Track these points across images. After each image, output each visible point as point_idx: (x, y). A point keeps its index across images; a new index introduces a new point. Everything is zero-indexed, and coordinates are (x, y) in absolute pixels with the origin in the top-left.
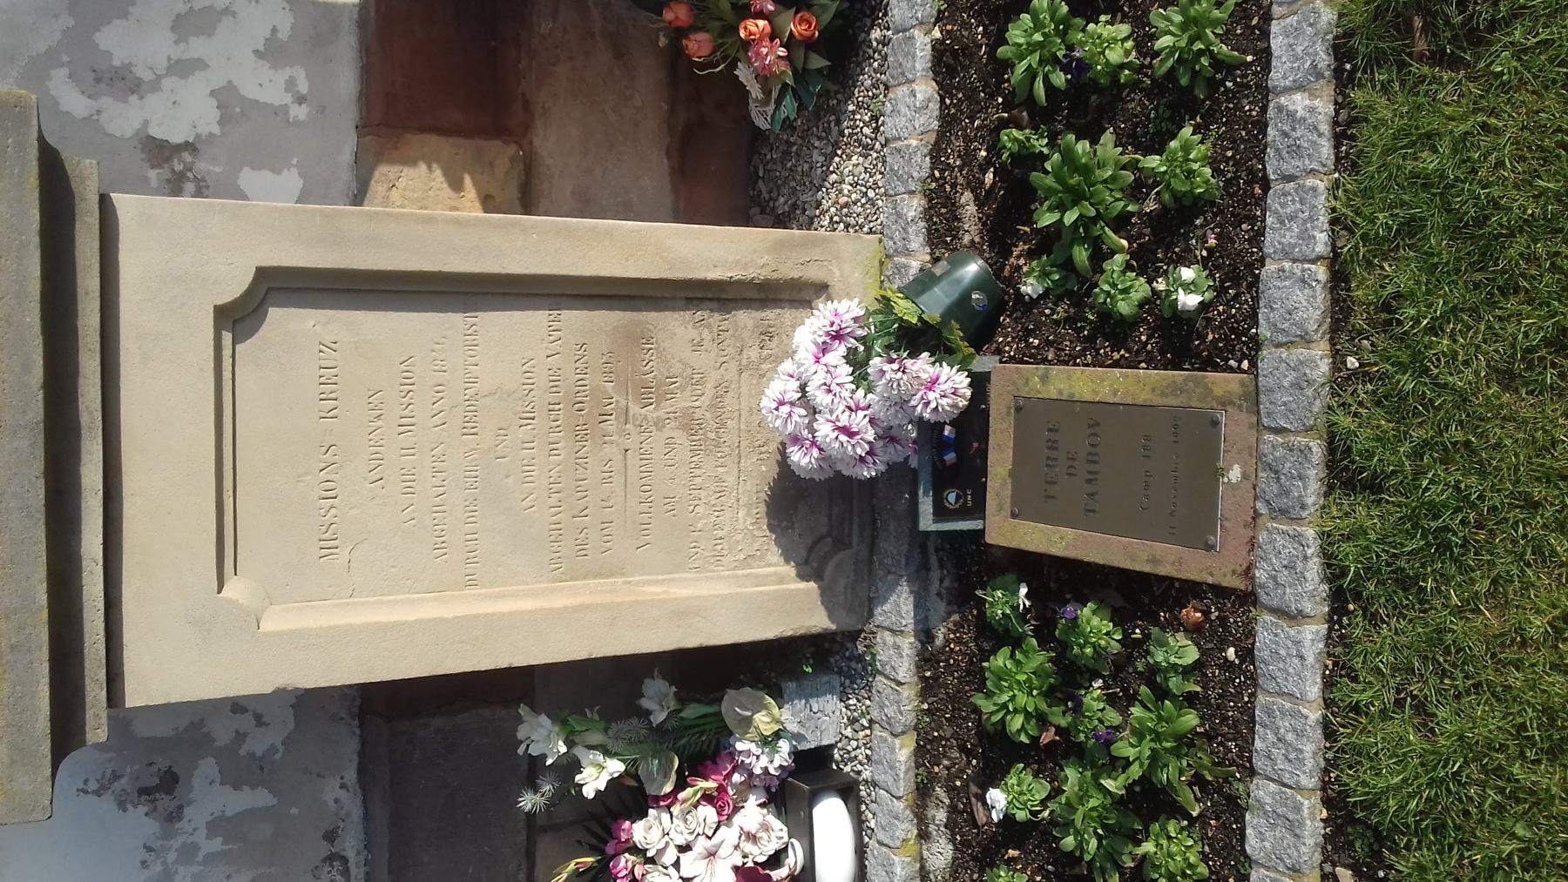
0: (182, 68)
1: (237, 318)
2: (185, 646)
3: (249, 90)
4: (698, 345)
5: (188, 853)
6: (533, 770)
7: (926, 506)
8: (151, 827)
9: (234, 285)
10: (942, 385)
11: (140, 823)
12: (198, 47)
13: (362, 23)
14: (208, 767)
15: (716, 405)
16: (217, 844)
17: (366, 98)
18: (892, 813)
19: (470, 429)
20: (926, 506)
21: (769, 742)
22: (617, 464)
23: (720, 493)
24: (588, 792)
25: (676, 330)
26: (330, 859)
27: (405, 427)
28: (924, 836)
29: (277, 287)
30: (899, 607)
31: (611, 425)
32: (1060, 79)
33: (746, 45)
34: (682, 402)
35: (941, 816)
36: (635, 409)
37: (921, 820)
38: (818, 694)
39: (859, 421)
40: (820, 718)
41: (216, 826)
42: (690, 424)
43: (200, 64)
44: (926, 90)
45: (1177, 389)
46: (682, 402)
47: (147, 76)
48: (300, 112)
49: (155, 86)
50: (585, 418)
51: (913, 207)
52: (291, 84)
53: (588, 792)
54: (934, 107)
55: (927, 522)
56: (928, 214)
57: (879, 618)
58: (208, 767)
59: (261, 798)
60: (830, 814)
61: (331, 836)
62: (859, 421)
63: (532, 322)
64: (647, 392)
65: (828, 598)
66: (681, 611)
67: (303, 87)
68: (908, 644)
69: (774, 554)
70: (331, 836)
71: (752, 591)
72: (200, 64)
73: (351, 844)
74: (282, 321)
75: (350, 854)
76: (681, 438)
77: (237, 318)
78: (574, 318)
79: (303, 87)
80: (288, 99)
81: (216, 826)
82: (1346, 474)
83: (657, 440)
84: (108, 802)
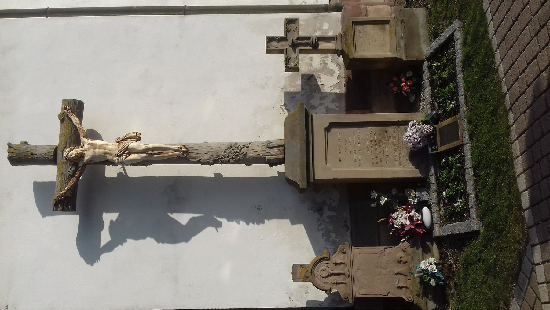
0: (321, 105)
1: (328, 129)
2: (323, 171)
3: (330, 107)
4: (394, 132)
5: (324, 221)
6: (374, 200)
7: (430, 149)
8: (319, 216)
9: (327, 125)
10: (428, 128)
11: (317, 215)
12: (323, 102)
13: (346, 96)
14: (326, 207)
15: (398, 141)
16: (328, 220)
17: (346, 106)
18: (435, 208)
19: (359, 144)
20: (430, 149)
21: (414, 198)
22: (382, 149)
23: (400, 154)
24: (382, 204)
25: (391, 130)
26: (345, 225)
27: (350, 143)
28: (440, 210)
29: (333, 125)
30: (432, 171)
31: (381, 144)
32: (440, 81)
33: (402, 87)
34: (392, 140)
35: (442, 205)
36: (384, 141)
37: (439, 207)
38: (423, 191)
39: (417, 137)
40: (425, 196)
41: (328, 217)
42: (394, 144)
43: (323, 104)
44: (429, 88)
45: (454, 119)
46: (392, 140)
47: (316, 106)
48: (337, 109)
49: (317, 107)
50: (376, 143)
51: (429, 106)
52: (336, 105)
53: (382, 204)
54: (430, 91)
55: (430, 152)
56: (431, 107)
57: (430, 174)
58: (326, 207)
59: (335, 214)
60: (425, 210)
61: (345, 222)
62: (417, 137)
63: (368, 129)
64: (386, 139)
65: (421, 171)
66: (394, 172)
67: (337, 105)
68: (434, 177)
69: (411, 165)
70: (345, 222)
71: (406, 170)
72: (323, 104)
73: (349, 223)
74: (333, 130)
75: (349, 225)
76: (392, 146)
77: (328, 129)
78: (373, 128)
79: (337, 105)
80: (335, 107)
81: (328, 217)
82: (469, 122)
83: (388, 146)
84: (312, 211)
